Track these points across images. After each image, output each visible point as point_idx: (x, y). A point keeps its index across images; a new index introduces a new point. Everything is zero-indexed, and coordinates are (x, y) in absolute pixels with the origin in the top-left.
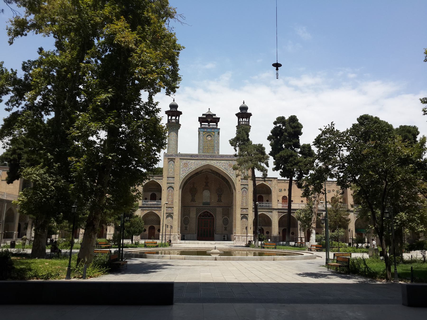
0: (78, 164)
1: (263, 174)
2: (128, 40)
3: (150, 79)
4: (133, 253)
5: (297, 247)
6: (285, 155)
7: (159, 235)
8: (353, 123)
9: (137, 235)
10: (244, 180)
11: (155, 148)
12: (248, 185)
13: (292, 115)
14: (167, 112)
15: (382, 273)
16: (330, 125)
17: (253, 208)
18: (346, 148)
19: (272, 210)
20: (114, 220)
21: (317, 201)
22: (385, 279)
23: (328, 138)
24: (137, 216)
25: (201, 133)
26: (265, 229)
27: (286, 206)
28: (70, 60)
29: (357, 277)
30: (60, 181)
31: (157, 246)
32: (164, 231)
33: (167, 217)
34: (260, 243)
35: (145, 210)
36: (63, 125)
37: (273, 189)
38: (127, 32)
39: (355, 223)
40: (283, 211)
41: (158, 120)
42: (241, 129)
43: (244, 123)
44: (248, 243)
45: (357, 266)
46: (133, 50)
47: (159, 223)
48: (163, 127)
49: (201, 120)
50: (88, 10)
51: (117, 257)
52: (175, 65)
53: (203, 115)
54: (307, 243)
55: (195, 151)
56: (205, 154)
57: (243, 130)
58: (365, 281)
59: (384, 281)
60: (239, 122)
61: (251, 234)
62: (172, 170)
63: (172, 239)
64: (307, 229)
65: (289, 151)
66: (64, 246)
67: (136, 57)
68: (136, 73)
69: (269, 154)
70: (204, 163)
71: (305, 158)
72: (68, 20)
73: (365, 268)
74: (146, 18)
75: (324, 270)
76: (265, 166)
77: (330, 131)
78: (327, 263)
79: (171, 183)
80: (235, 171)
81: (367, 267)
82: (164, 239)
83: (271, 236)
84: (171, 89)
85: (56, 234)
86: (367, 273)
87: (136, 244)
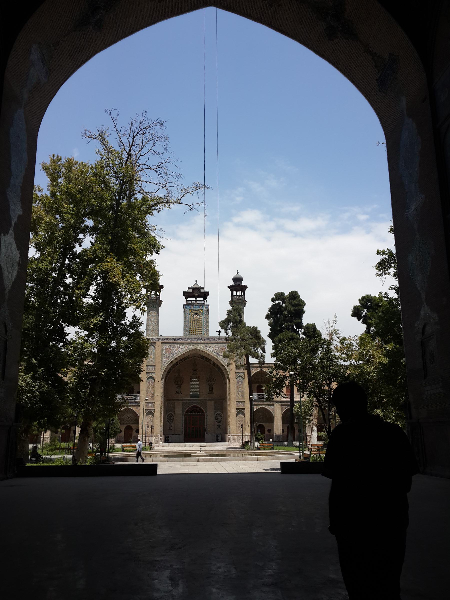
7: (138, 437)
8: (355, 305)
9: (112, 438)
13: (293, 290)
26: (267, 426)
32: (144, 432)
33: (147, 414)
47: (137, 423)
49: (187, 295)
53: (189, 288)
55: (181, 334)
56: (192, 336)
60: (232, 297)
61: (248, 433)
63: (153, 441)
70: (191, 347)
79: (152, 373)
83: (273, 435)
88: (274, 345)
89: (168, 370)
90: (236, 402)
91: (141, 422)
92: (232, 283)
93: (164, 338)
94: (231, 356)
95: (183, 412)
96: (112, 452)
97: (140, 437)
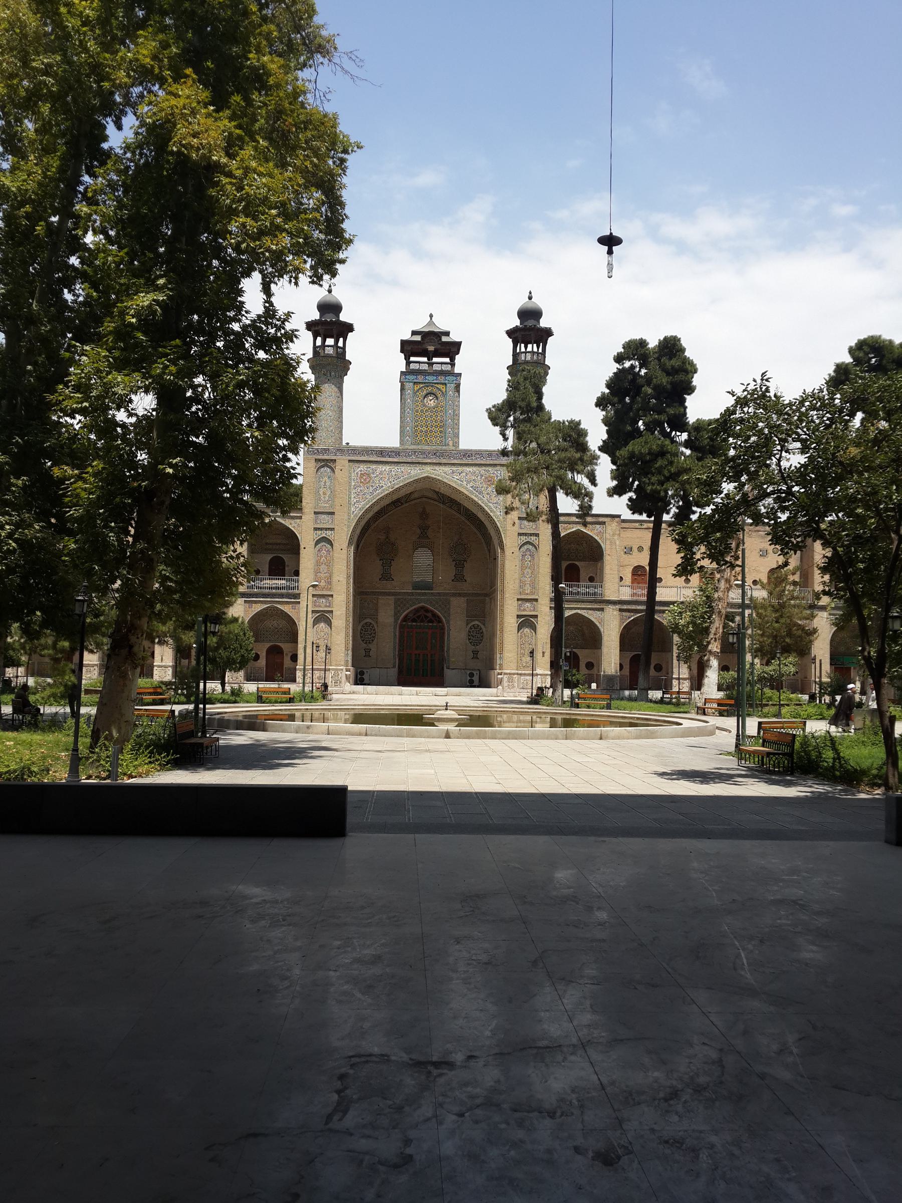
0: (81, 486)
1: (581, 507)
2: (209, 143)
3: (268, 250)
4: (226, 717)
5: (669, 703)
6: (645, 450)
7: (295, 669)
8: (839, 361)
9: (237, 670)
10: (525, 522)
11: (286, 442)
12: (537, 535)
14: (310, 326)
15: (874, 772)
16: (759, 381)
17: (551, 600)
18: (798, 445)
19: (602, 603)
20: (175, 629)
21: (728, 581)
22: (883, 788)
23: (751, 417)
24: (235, 620)
25: (409, 386)
26: (584, 655)
27: (642, 594)
28: (40, 184)
29: (810, 783)
30: (30, 526)
31: (291, 700)
32: (309, 659)
33: (316, 622)
34: (567, 692)
35: (256, 602)
36: (30, 371)
37: (608, 547)
38: (201, 121)
39: (832, 640)
40: (634, 607)
41: (291, 365)
42: (520, 377)
43: (529, 357)
44: (535, 692)
45: (814, 754)
46: (217, 167)
47: (295, 640)
48: (305, 384)
49: (409, 348)
50: (85, 33)
51: (192, 727)
52: (334, 202)
53: (414, 333)
54: (696, 694)
55: (392, 440)
57: (525, 379)
58: (828, 792)
59: (878, 792)
60: (515, 355)
61: (543, 669)
62: (328, 493)
63: (329, 681)
64: (696, 658)
65: (656, 441)
66: (49, 697)
67: (229, 187)
68: (230, 233)
69: (600, 449)
71: (699, 459)
72: (33, 68)
73: (834, 759)
74: (253, 69)
75: (730, 764)
76: (586, 482)
77: (759, 397)
78: (737, 746)
79: (326, 529)
80: (501, 498)
81: (838, 757)
82: (308, 680)
84: (326, 265)
85: (16, 664)
86: (838, 773)
87: (235, 694)
88: (614, 467)
89: (363, 523)
90: (518, 600)
91: (301, 638)
92: (516, 322)
93: (355, 450)
94: (515, 488)
95: (396, 621)
96: (235, 702)
97: (300, 670)
